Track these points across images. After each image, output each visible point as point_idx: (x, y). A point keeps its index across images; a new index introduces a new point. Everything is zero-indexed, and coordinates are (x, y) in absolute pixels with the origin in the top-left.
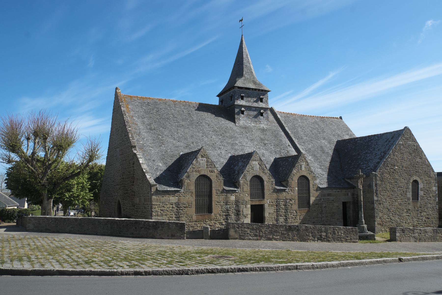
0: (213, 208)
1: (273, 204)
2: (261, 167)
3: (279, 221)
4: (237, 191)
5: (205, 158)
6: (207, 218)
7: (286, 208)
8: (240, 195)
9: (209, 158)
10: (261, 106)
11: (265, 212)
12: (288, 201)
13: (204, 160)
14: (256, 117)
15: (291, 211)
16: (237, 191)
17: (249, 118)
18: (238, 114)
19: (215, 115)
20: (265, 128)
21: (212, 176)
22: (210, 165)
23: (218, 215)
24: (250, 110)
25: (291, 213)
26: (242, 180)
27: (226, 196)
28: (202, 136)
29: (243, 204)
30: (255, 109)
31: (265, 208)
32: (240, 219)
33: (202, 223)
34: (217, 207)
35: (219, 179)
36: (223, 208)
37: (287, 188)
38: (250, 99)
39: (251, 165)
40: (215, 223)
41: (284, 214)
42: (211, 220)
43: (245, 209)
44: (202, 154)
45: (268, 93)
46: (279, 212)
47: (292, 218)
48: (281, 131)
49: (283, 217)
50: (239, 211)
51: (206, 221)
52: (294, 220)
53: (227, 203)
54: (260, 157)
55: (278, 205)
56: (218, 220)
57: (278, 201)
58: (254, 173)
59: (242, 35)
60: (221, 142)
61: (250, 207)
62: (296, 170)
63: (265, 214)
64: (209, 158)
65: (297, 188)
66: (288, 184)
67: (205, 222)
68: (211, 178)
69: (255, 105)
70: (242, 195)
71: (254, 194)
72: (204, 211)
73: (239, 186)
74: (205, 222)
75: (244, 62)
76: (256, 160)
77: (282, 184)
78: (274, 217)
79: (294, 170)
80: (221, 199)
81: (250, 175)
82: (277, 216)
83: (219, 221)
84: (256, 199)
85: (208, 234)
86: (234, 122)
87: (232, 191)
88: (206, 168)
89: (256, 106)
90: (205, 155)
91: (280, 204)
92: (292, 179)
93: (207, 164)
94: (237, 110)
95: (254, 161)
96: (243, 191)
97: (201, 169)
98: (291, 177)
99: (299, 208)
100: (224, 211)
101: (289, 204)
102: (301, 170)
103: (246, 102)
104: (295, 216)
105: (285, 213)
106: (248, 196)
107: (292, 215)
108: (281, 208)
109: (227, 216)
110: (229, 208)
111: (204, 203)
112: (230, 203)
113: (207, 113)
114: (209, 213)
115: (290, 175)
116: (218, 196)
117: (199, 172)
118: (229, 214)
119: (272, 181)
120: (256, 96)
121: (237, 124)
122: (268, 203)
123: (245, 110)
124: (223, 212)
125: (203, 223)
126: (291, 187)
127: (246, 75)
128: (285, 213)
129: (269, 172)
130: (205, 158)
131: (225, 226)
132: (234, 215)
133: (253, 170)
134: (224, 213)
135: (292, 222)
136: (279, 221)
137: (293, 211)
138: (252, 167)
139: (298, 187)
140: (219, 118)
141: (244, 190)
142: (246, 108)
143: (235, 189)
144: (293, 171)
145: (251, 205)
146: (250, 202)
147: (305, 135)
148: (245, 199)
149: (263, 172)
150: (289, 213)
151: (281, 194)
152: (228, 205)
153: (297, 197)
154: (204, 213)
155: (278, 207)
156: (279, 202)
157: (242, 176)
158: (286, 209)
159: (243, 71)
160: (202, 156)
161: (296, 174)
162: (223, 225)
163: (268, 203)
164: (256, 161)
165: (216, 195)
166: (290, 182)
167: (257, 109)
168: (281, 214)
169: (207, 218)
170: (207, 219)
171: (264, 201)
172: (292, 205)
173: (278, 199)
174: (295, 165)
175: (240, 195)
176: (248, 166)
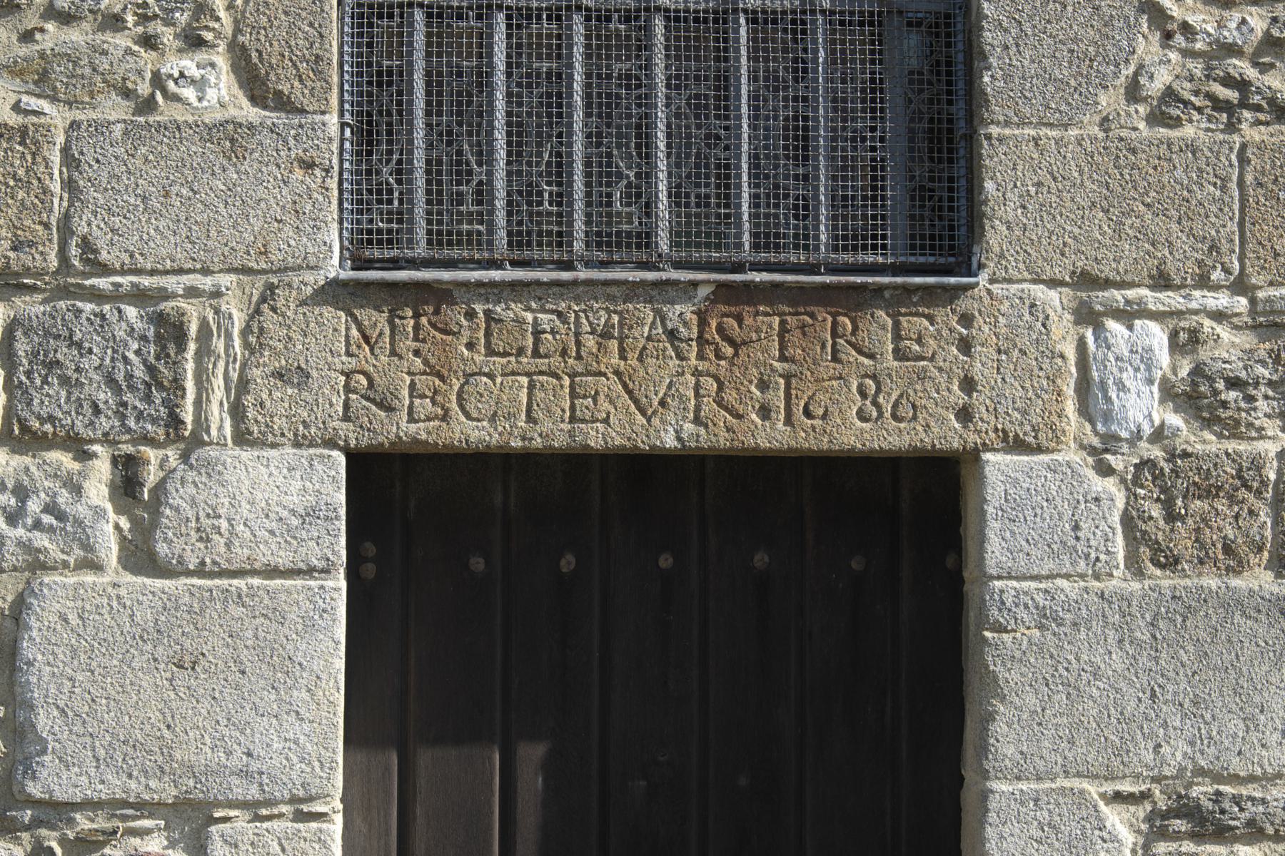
171: (946, 317)
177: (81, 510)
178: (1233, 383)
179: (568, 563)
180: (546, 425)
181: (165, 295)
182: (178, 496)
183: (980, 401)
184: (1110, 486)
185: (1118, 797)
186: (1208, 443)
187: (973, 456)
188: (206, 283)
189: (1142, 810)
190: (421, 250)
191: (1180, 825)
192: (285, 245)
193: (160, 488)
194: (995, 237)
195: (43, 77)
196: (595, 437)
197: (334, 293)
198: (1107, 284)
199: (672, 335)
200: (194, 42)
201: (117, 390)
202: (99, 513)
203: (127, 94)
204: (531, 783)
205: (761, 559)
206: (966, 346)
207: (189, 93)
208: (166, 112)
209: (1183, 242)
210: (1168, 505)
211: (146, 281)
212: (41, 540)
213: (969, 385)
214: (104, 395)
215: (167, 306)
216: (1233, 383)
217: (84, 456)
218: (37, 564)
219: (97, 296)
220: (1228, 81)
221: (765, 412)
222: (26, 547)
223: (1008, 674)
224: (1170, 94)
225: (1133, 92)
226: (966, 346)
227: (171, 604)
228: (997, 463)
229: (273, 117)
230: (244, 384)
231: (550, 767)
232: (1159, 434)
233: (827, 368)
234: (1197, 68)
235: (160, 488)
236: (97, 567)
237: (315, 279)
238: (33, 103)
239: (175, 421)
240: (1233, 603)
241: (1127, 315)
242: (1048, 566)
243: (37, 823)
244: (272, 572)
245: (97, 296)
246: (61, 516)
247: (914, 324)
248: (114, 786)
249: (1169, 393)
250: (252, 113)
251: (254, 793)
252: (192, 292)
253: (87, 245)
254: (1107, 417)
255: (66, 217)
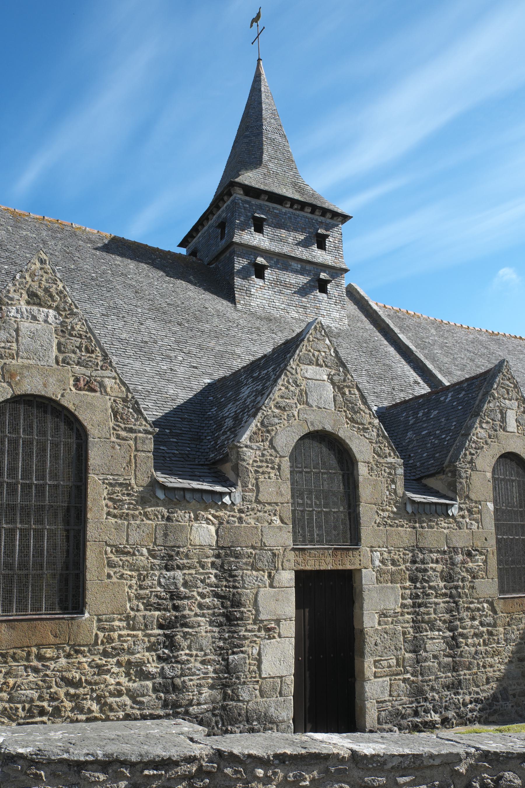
0: (89, 585)
1: (399, 572)
2: (343, 394)
3: (426, 651)
4: (227, 500)
5: (52, 312)
6: (52, 639)
7: (454, 591)
8: (240, 519)
9: (73, 314)
10: (320, 260)
11: (365, 606)
12: (459, 558)
13: (46, 321)
14: (303, 291)
15: (472, 603)
16: (227, 500)
17: (280, 292)
18: (245, 274)
19: (164, 272)
20: (333, 328)
21: (91, 406)
22: (79, 348)
23: (117, 623)
24: (286, 268)
25: (473, 611)
26: (254, 445)
27: (169, 519)
28: (103, 315)
29: (260, 565)
30: (301, 267)
31: (361, 591)
32: (242, 646)
33: (19, 667)
34: (114, 580)
35: (131, 430)
36: (148, 582)
37: (456, 500)
38: (283, 233)
39: (295, 382)
40: (101, 670)
41: (447, 616)
42: (77, 652)
43: (265, 592)
44: (35, 285)
45: (344, 228)
46: (422, 609)
47: (476, 635)
48: (386, 342)
49: (439, 630)
50: (237, 603)
51: (40, 658)
52: (485, 644)
53: (171, 557)
54: (336, 352)
55: (420, 575)
56: (118, 652)
57: (420, 556)
58: (311, 417)
59: (259, 60)
60: (177, 342)
61: (293, 584)
62: (484, 425)
63: (366, 619)
64: (75, 314)
65: (491, 506)
66: (459, 487)
67: (35, 663)
68: (83, 416)
69: (301, 253)
70: (252, 522)
71: (310, 520)
72: (37, 600)
73: (238, 475)
74: (39, 665)
75: (264, 127)
76: (321, 362)
77: (425, 485)
78: (404, 633)
79: (478, 425)
80: (135, 537)
81: (290, 426)
82: (417, 629)
83: (124, 658)
84: (320, 542)
85: (459, 497)
86: (232, 300)
87: (197, 496)
88: (52, 362)
89: (304, 258)
90: (51, 296)
91: (425, 570)
92: (471, 462)
93: (59, 344)
94: (240, 263)
95: (310, 363)
96: (257, 501)
97: (26, 362)
98: (469, 457)
99: (502, 591)
100: (153, 600)
101: (464, 574)
102: (504, 430)
103: (271, 240)
104: (489, 625)
105: (449, 611)
106: (280, 528)
107: (477, 623)
108: (430, 587)
109: (168, 628)
110: (185, 584)
111: (39, 552)
112: (187, 556)
113: (136, 262)
114: (65, 609)
115: (462, 446)
116: (121, 517)
117: (12, 376)
118: (184, 617)
119: (392, 466)
120: (305, 228)
121: (239, 306)
122: (377, 563)
123: (267, 264)
124: (148, 606)
125: (26, 667)
126: (468, 497)
127: (271, 165)
128: (449, 611)
129: (376, 421)
130: (50, 307)
131: (159, 680)
132: (211, 623)
133: (307, 404)
134: (157, 613)
135: (476, 653)
136: (426, 651)
137: (479, 603)
138: (301, 391)
139: (495, 503)
140: (179, 281)
141: (261, 498)
142: (271, 259)
143: (218, 488)
144: (474, 431)
145: (296, 572)
146: (291, 555)
147: (457, 366)
148: (269, 541)
149: (352, 420)
150: (465, 614)
151: (432, 527)
152: (179, 568)
153: (492, 542)
154: (37, 609)
155: (418, 585)
156: (423, 562)
157: (254, 424)
158: (451, 596)
159: (262, 153)
160: (32, 295)
161: (487, 443)
162: (145, 676)
163: (377, 563)
164: (318, 365)
165: (108, 514)
166: (463, 475)
167: (308, 267)
168: (433, 616)
169: (52, 639)
170: (49, 646)
171: (356, 553)
172: (474, 577)
173: (421, 550)
174: (480, 407)
175: (240, 519)
176: (280, 382)
177: (264, 580)
178: (387, 560)
179: (310, 584)
180: (316, 567)
181: (273, 550)
182: (276, 577)
183: (362, 562)
184: (374, 573)
185: (377, 613)
186: (384, 567)
187: (360, 570)
188: (278, 548)
189: (378, 614)
190: (30, 612)
191: (382, 616)
192: (287, 543)
193: (274, 576)
194: (362, 541)
195: (258, 519)
196: (322, 568)
197: (293, 549)
198: (374, 547)
199: (329, 554)
200: (275, 515)
201: (268, 563)
202: (266, 580)
203: (268, 522)
204: (307, 614)
205: (331, 583)
206: (360, 555)
207: (275, 522)
208: (273, 525)
209: (381, 542)
210: (380, 575)
211: (271, 548)
212: (260, 584)
213: (360, 560)
214: (267, 563)
215: (274, 551)
216: (387, 560)
217: (264, 572)
218: (259, 587)
219: (265, 550)
220: (385, 521)
221: (339, 564)
222: (258, 585)
223: (365, 598)
224: (379, 523)
225: (375, 523)
226: (360, 555)
227: (275, 592)
228: (364, 570)
229: (285, 526)
230: (283, 562)
231: (309, 612)
232: (379, 566)
233: (346, 559)
234: (381, 519)
235: (274, 576)
236: (266, 587)
237: (291, 547)
238: (257, 523)
239: (275, 567)
240: (387, 587)
241: (376, 551)
242: (369, 583)
243: (259, 623)
244: (287, 587)
245: (265, 550)
246: (262, 580)
247: (354, 553)
248: (269, 617)
249: (380, 561)
250: (282, 525)
251: (285, 618)
252: (277, 549)
253: (264, 543)
254: (374, 564)
255: (262, 539)
